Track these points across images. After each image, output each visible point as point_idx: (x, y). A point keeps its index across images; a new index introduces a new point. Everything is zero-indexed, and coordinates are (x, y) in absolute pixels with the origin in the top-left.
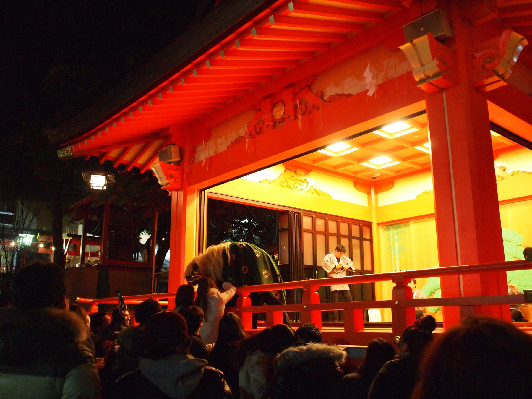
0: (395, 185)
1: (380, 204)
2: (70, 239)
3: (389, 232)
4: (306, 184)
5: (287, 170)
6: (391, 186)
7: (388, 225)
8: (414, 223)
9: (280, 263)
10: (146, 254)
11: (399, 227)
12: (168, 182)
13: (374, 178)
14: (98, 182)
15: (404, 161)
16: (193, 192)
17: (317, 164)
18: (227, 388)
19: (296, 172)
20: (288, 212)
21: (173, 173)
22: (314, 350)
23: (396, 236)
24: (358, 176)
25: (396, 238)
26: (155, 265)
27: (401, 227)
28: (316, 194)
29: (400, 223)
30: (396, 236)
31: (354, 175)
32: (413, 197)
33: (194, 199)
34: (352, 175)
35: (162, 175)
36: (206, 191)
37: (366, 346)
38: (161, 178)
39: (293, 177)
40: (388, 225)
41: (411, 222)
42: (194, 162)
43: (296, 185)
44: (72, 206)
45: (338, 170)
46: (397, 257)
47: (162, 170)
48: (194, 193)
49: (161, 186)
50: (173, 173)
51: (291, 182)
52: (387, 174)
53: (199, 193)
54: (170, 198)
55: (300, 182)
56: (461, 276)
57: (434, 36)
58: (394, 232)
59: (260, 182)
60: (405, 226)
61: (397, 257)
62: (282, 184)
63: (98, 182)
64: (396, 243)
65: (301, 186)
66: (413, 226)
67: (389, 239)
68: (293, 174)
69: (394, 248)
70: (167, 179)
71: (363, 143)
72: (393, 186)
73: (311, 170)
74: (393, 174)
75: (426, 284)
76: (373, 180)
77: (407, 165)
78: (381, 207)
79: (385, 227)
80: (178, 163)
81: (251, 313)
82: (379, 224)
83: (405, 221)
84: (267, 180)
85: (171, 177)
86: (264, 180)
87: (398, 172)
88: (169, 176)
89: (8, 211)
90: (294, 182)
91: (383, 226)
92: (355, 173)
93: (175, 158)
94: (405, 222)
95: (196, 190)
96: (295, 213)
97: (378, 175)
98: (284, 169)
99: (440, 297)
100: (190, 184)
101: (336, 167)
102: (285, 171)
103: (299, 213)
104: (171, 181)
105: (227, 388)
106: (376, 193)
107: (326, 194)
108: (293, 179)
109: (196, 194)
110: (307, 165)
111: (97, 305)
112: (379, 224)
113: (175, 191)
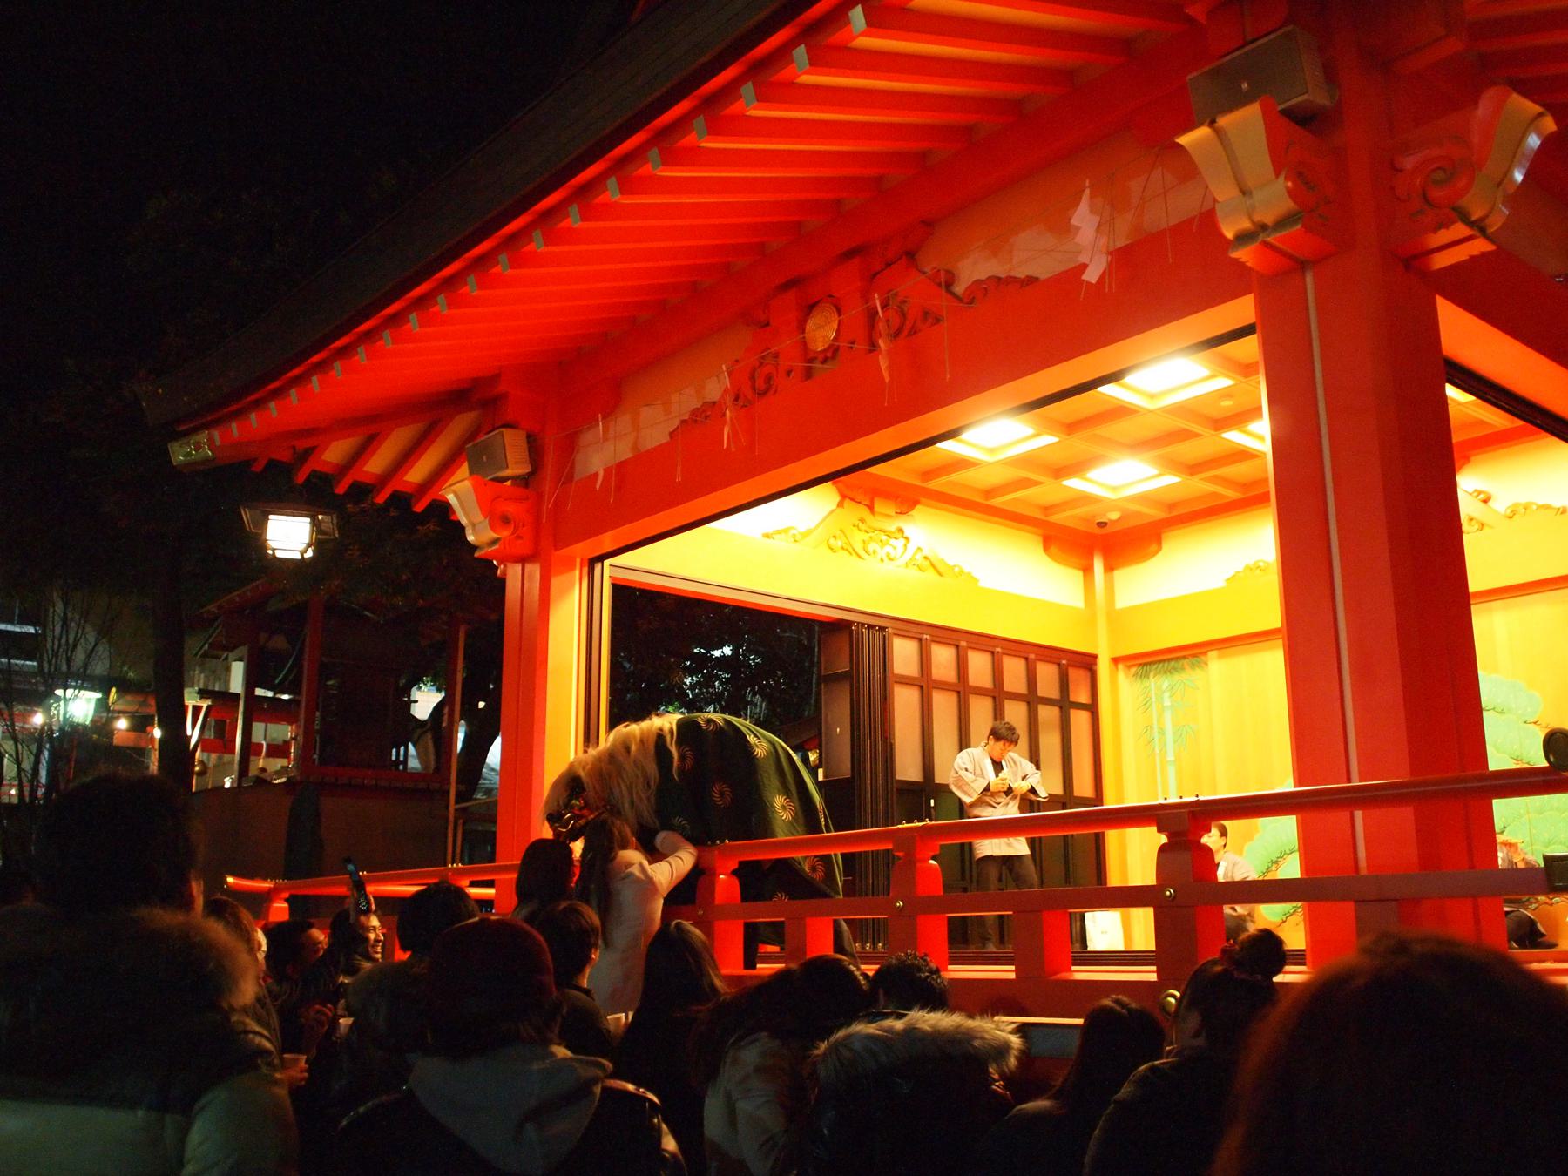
0: (1165, 546)
1: (1121, 603)
2: (205, 704)
3: (1146, 683)
4: (903, 541)
5: (847, 502)
6: (1154, 547)
7: (1145, 662)
8: (1220, 657)
9: (825, 776)
10: (431, 749)
11: (1175, 669)
12: (495, 536)
13: (1102, 525)
14: (289, 536)
15: (1192, 474)
16: (570, 566)
17: (935, 484)
18: (670, 1144)
19: (871, 508)
20: (849, 624)
21: (511, 509)
22: (925, 1033)
23: (1167, 695)
24: (1056, 518)
25: (1167, 703)
26: (458, 782)
27: (1183, 668)
28: (931, 573)
29: (1178, 659)
30: (1167, 695)
31: (1042, 517)
32: (1218, 582)
33: (573, 585)
34: (1038, 515)
35: (478, 517)
36: (607, 563)
37: (1080, 1021)
38: (474, 526)
39: (862, 521)
40: (1145, 662)
41: (1213, 654)
42: (570, 477)
43: (872, 546)
44: (212, 608)
45: (997, 502)
46: (1171, 757)
47: (479, 501)
48: (572, 569)
49: (474, 548)
50: (511, 509)
51: (858, 538)
52: (1139, 514)
53: (585, 570)
54: (502, 583)
55: (883, 537)
56: (1358, 814)
57: (1280, 107)
58: (1160, 684)
59: (767, 536)
60: (1193, 666)
61: (1171, 757)
62: (832, 541)
63: (289, 536)
64: (1168, 715)
65: (888, 549)
66: (1217, 665)
67: (1146, 704)
68: (865, 512)
69: (1162, 732)
70: (493, 527)
71: (1069, 420)
72: (1160, 548)
73: (916, 502)
74: (1157, 514)
75: (1257, 837)
76: (1098, 531)
77: (1199, 485)
78: (1122, 610)
79: (1134, 670)
80: (524, 481)
81: (741, 923)
82: (1116, 661)
83: (1194, 652)
84: (786, 531)
85: (505, 521)
86: (778, 532)
87: (1172, 506)
88: (498, 520)
89: (22, 622)
90: (866, 536)
91: (1130, 667)
92: (1047, 509)
93: (516, 466)
94: (1194, 656)
95: (578, 561)
96: (871, 627)
97: (1114, 516)
98: (837, 498)
99: (1298, 876)
100: (560, 542)
101: (990, 492)
102: (840, 505)
103: (882, 629)
104: (505, 533)
105: (670, 1144)
106: (1109, 568)
107: (961, 573)
108: (862, 527)
109: (577, 573)
110: (906, 486)
111: (286, 900)
112: (1116, 661)
113: (516, 562)
